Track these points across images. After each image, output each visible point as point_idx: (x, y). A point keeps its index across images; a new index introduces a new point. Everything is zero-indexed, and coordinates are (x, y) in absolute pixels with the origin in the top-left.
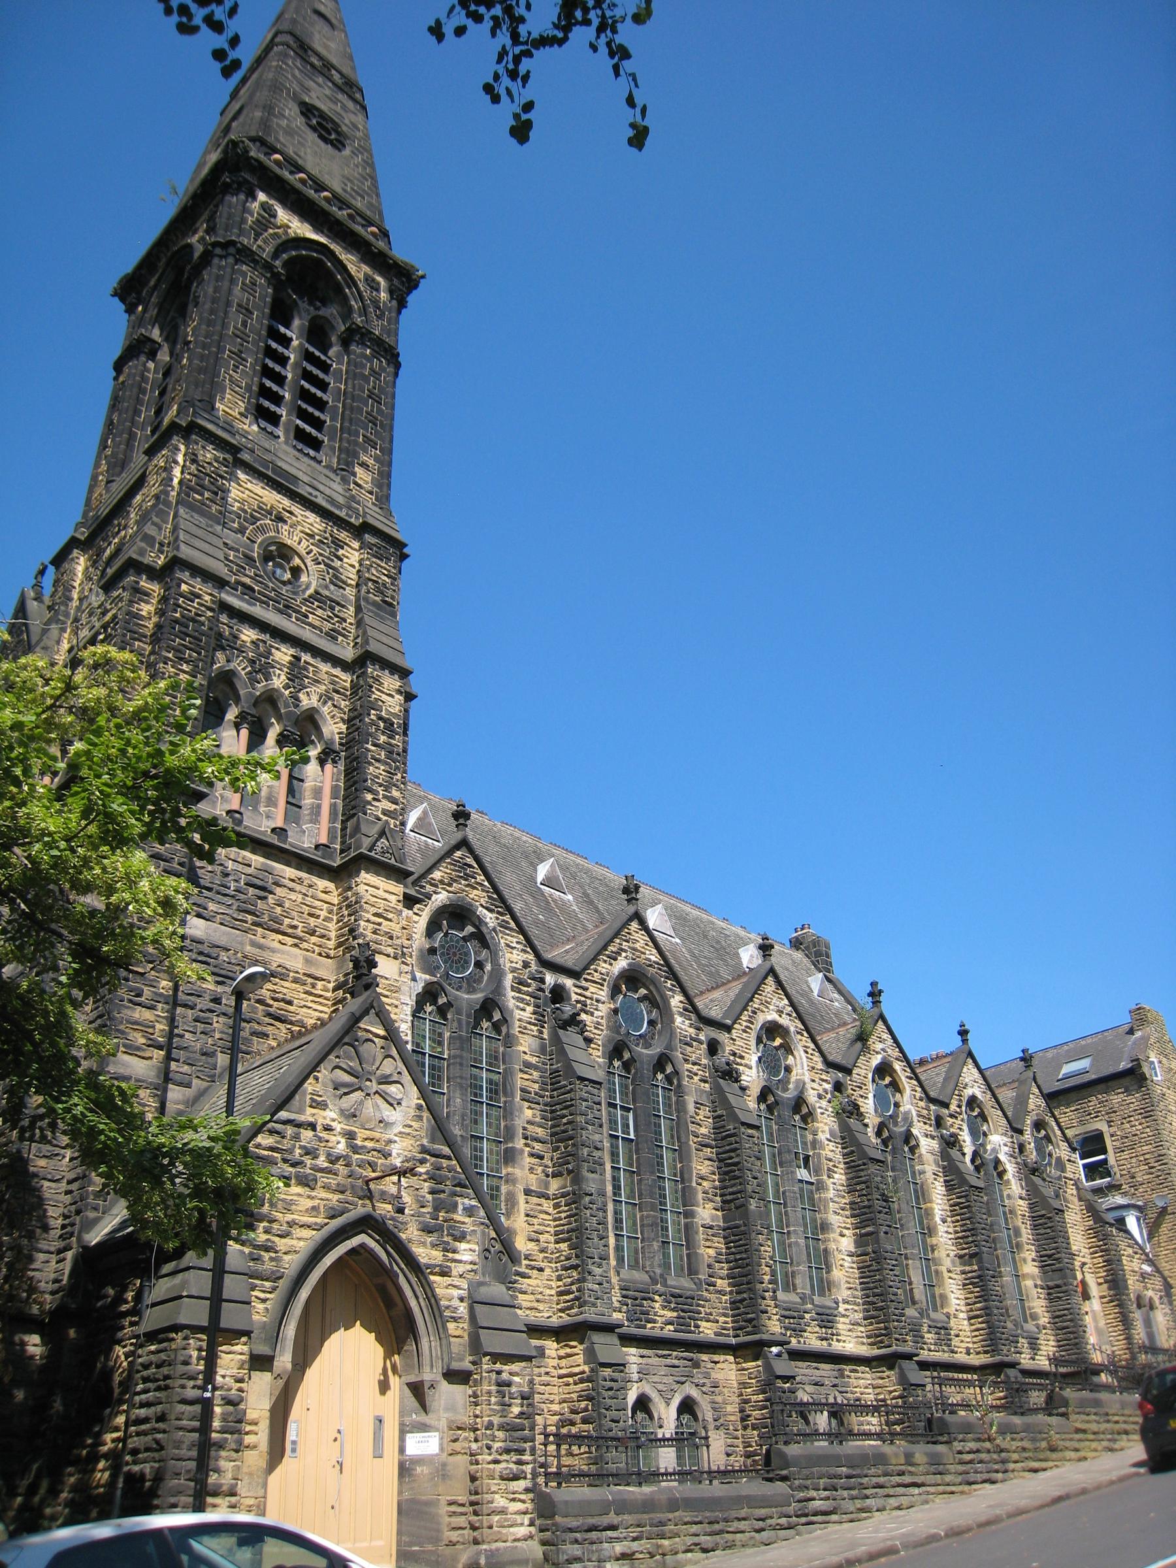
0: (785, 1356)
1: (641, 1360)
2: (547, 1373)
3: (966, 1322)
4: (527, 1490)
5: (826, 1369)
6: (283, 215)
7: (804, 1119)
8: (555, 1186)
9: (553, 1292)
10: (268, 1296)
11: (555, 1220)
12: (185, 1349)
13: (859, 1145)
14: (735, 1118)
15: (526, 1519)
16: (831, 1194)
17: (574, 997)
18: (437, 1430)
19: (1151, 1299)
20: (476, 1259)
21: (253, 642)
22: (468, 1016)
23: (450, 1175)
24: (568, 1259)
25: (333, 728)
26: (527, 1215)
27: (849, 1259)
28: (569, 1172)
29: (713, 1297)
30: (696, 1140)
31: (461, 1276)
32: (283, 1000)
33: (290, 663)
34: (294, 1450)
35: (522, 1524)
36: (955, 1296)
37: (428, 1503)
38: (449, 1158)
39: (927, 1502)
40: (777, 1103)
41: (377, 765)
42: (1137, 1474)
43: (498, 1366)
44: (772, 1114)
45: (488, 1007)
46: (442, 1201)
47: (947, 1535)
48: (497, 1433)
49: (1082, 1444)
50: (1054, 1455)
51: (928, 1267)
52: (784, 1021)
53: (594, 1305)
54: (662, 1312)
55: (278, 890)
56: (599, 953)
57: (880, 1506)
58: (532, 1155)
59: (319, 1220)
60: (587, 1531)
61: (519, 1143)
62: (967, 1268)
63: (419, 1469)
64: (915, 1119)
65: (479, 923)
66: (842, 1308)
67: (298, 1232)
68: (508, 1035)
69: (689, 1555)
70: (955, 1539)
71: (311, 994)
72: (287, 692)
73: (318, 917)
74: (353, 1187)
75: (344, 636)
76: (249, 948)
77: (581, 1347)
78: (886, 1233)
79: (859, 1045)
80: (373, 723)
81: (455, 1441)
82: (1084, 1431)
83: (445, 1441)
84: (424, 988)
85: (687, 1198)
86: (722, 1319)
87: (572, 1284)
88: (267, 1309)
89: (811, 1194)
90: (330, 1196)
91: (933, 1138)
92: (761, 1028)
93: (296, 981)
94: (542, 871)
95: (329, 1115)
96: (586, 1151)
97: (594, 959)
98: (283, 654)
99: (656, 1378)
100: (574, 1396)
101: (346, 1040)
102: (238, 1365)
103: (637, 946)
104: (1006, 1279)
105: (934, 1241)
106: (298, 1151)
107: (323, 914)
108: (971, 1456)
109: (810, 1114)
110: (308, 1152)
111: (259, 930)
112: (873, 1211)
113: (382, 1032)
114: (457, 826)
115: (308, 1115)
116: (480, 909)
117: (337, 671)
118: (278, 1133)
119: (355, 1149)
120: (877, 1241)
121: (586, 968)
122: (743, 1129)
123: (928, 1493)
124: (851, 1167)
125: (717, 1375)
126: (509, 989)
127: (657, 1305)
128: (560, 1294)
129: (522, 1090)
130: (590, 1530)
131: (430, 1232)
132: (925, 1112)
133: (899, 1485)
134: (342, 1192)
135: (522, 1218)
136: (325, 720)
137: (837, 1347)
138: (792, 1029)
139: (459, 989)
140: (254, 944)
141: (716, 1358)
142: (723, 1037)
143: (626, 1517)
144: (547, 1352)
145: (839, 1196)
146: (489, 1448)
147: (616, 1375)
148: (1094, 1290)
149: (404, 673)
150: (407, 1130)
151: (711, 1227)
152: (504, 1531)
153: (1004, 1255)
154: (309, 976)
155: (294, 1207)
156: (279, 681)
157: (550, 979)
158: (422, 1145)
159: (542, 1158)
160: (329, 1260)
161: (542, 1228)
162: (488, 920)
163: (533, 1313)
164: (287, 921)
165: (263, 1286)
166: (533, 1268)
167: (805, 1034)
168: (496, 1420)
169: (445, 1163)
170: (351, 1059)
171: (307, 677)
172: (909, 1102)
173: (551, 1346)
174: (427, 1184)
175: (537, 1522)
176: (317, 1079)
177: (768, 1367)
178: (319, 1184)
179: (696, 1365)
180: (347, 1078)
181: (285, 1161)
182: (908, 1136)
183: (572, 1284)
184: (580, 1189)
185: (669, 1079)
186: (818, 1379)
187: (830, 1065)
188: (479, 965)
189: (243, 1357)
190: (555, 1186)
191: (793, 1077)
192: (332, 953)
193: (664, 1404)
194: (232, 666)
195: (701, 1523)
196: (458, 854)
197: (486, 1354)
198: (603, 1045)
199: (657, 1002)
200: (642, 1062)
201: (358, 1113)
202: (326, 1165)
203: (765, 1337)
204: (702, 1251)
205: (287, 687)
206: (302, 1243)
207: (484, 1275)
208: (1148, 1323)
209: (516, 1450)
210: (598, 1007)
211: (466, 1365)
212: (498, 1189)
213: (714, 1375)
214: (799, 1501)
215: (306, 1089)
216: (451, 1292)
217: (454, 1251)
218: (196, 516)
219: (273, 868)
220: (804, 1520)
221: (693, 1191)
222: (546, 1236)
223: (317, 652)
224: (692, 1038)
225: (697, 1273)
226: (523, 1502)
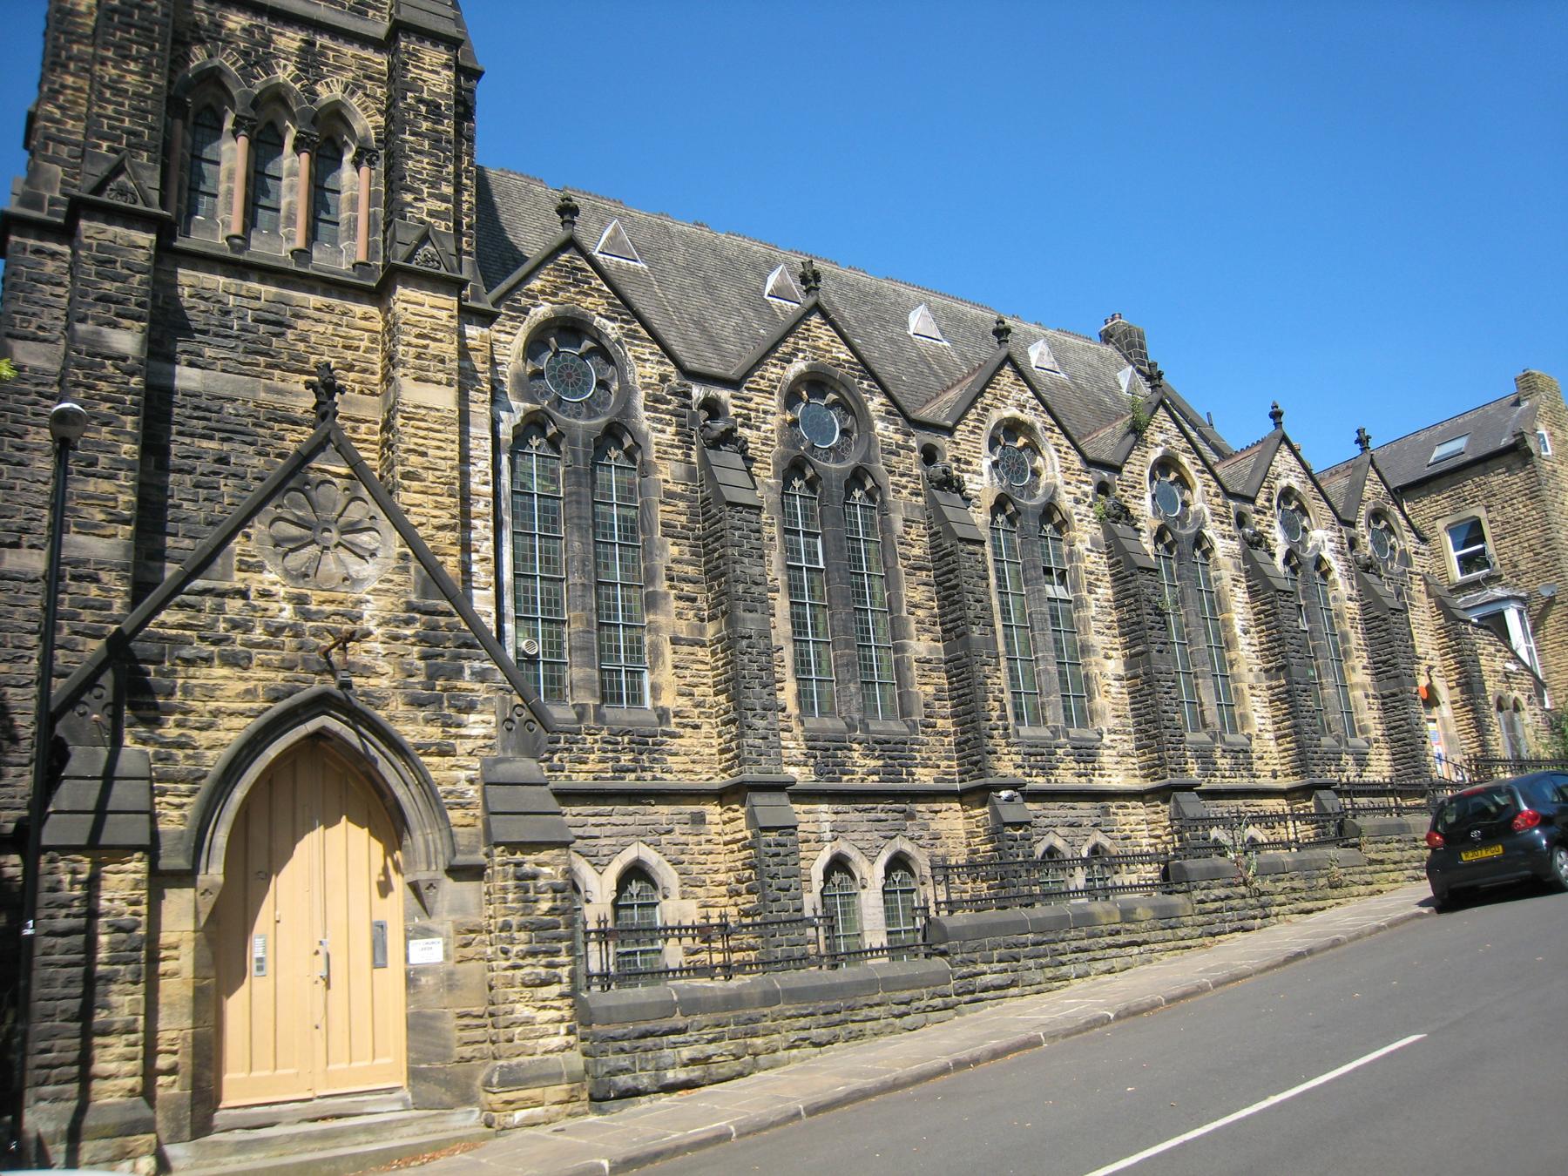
0: (1020, 799)
1: (834, 817)
2: (709, 841)
3: (1272, 743)
4: (562, 996)
5: (1084, 808)
7: (1058, 528)
8: (711, 630)
9: (714, 751)
10: (185, 800)
11: (713, 669)
12: (51, 873)
13: (1126, 553)
14: (952, 533)
15: (563, 1029)
16: (1093, 611)
17: (732, 410)
18: (440, 935)
19: (1516, 699)
20: (491, 730)
21: (244, 29)
22: (586, 445)
23: (451, 635)
24: (726, 713)
25: (366, 122)
26: (676, 667)
27: (1117, 683)
28: (724, 613)
29: (932, 740)
31: (470, 754)
33: (300, 49)
34: (260, 968)
35: (557, 1034)
36: (1258, 713)
37: (434, 1017)
38: (450, 614)
39: (1150, 961)
40: (1018, 512)
41: (418, 157)
42: (1419, 915)
43: (518, 857)
45: (614, 433)
46: (440, 667)
47: (1118, 1017)
48: (516, 935)
49: (1376, 876)
50: (1336, 892)
51: (1226, 686)
52: (1027, 416)
53: (757, 762)
54: (862, 762)
55: (300, 324)
56: (766, 355)
57: (1081, 972)
58: (679, 598)
59: (255, 706)
60: (638, 1038)
61: (662, 586)
62: (1274, 683)
63: (423, 980)
64: (1208, 518)
65: (597, 335)
66: (1107, 739)
67: (225, 722)
68: (642, 463)
69: (795, 1051)
70: (1132, 1019)
72: (298, 86)
73: (357, 349)
74: (305, 661)
75: (376, 8)
76: (263, 395)
77: (743, 810)
78: (1160, 651)
79: (1131, 438)
80: (410, 108)
81: (466, 945)
82: (1382, 862)
83: (452, 947)
84: (523, 419)
85: (897, 630)
86: (944, 764)
87: (731, 740)
88: (184, 816)
89: (1063, 617)
90: (272, 675)
91: (1232, 538)
92: (997, 426)
94: (772, 280)
95: (271, 578)
96: (740, 588)
97: (760, 363)
98: (289, 40)
99: (855, 836)
100: (739, 864)
101: (292, 484)
102: (131, 885)
103: (820, 343)
104: (1330, 691)
105: (1233, 655)
106: (222, 626)
107: (363, 345)
108: (1217, 904)
109: (1065, 521)
110: (235, 625)
111: (277, 372)
112: (1141, 626)
113: (344, 470)
115: (237, 580)
116: (598, 318)
117: (368, 53)
118: (191, 606)
119: (308, 616)
120: (1149, 662)
121: (748, 374)
122: (961, 546)
123: (1152, 951)
124: (1118, 579)
125: (937, 825)
126: (641, 409)
127: (856, 755)
128: (722, 752)
129: (663, 524)
130: (644, 1036)
131: (421, 705)
132: (1222, 510)
133: (1110, 946)
134: (290, 669)
135: (669, 670)
136: (355, 114)
137: (1100, 783)
138: (1039, 425)
139: (577, 415)
140: (269, 390)
141: (936, 807)
142: (943, 442)
143: (698, 1017)
144: (708, 818)
145: (1103, 613)
146: (505, 952)
147: (783, 839)
148: (1444, 694)
149: (453, 43)
150: (386, 586)
151: (929, 661)
152: (530, 1043)
153: (1326, 665)
155: (218, 693)
156: (285, 73)
157: (698, 392)
158: (408, 603)
159: (694, 600)
160: (273, 751)
161: (695, 680)
162: (609, 331)
163: (688, 776)
165: (176, 789)
166: (685, 726)
167: (1057, 430)
168: (515, 920)
169: (443, 621)
170: (300, 507)
171: (326, 65)
172: (1201, 498)
173: (713, 811)
174: (416, 649)
175: (578, 1030)
176: (248, 536)
177: (995, 813)
178: (255, 662)
179: (911, 816)
180: (295, 531)
181: (202, 639)
182: (1199, 540)
183: (731, 740)
184: (734, 632)
185: (870, 495)
186: (1073, 820)
187: (1090, 463)
188: (603, 385)
189: (138, 876)
190: (711, 630)
191: (1043, 482)
192: (378, 389)
193: (867, 863)
194: (216, 62)
195: (812, 1014)
196: (564, 257)
197: (497, 845)
198: (775, 464)
199: (851, 408)
200: (829, 480)
201: (311, 572)
202: (264, 638)
203: (990, 780)
204: (916, 688)
205: (296, 79)
206: (232, 735)
207: (504, 749)
208: (1511, 727)
209: (545, 952)
210: (765, 421)
211: (479, 858)
212: (639, 640)
213: (933, 826)
214: (960, 978)
215: (233, 550)
216: (456, 775)
217: (459, 726)
219: (291, 297)
220: (967, 998)
221: (905, 622)
222: (703, 688)
223: (336, 32)
224: (898, 446)
225: (910, 714)
226: (559, 1009)
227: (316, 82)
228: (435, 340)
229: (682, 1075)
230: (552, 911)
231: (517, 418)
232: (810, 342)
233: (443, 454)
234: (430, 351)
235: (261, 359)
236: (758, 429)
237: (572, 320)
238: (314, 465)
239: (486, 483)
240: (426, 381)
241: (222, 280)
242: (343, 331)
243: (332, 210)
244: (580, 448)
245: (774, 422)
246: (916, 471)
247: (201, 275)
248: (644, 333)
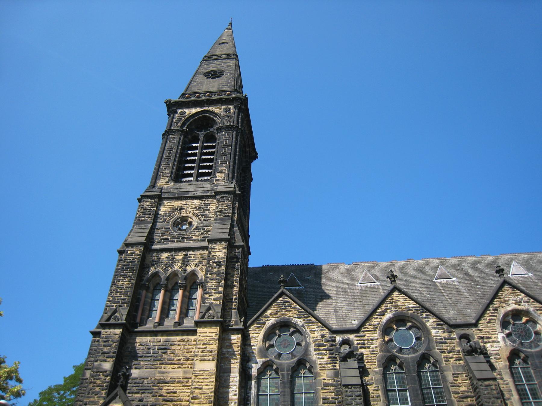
6: (187, 111)
17: (356, 342)
22: (288, 371)
30: (456, 396)
32: (171, 392)
33: (183, 258)
44: (528, 364)
45: (302, 363)
65: (295, 326)
71: (185, 386)
76: (157, 375)
84: (262, 365)
93: (178, 382)
103: (399, 303)
111: (163, 366)
114: (499, 276)
116: (294, 319)
122: (480, 383)
129: (323, 399)
138: (531, 309)
140: (159, 373)
142: (472, 331)
154: (185, 378)
157: (339, 338)
162: (299, 323)
164: (176, 358)
194: (157, 270)
199: (420, 327)
218: (141, 225)
219: (170, 339)
224: (445, 339)
227: (186, 266)
228: (209, 345)
231: (259, 365)
232: (394, 304)
233: (208, 387)
234: (207, 349)
235: (158, 362)
236: (369, 348)
237: (284, 322)
239: (235, 395)
240: (204, 360)
241: (149, 338)
242: (186, 347)
243: (194, 305)
244: (285, 372)
245: (377, 343)
246: (457, 349)
247: (143, 338)
248: (314, 320)
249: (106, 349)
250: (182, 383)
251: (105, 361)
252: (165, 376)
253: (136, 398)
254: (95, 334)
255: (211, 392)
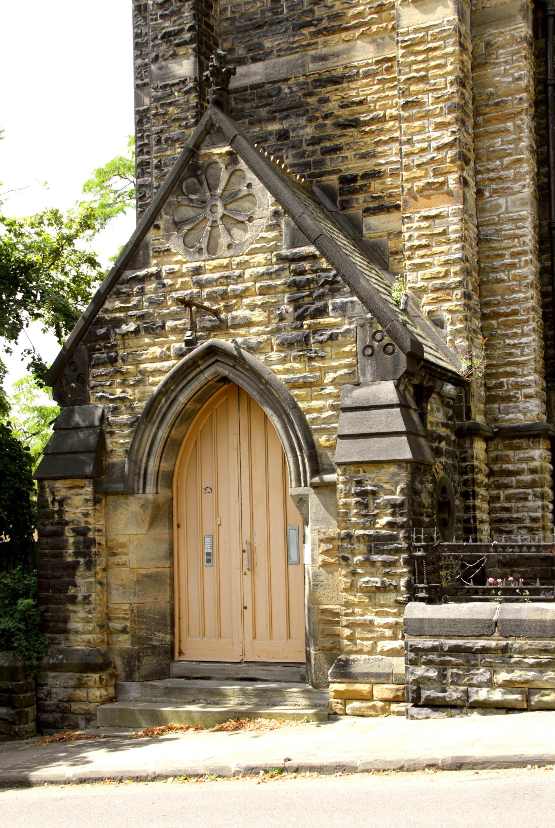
76: (311, 66)
93: (367, 75)
229: (497, 695)
230: (390, 525)
238: (203, 152)
249: (169, 26)
250: (377, 74)
251: (174, 56)
252: (329, 64)
253: (271, 133)
254: (5, 372)
255: (452, 83)
